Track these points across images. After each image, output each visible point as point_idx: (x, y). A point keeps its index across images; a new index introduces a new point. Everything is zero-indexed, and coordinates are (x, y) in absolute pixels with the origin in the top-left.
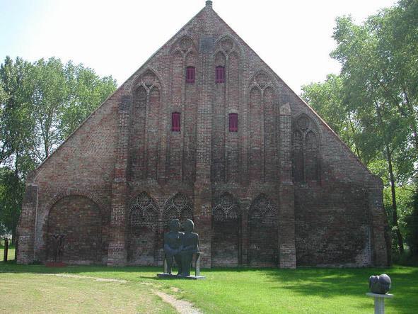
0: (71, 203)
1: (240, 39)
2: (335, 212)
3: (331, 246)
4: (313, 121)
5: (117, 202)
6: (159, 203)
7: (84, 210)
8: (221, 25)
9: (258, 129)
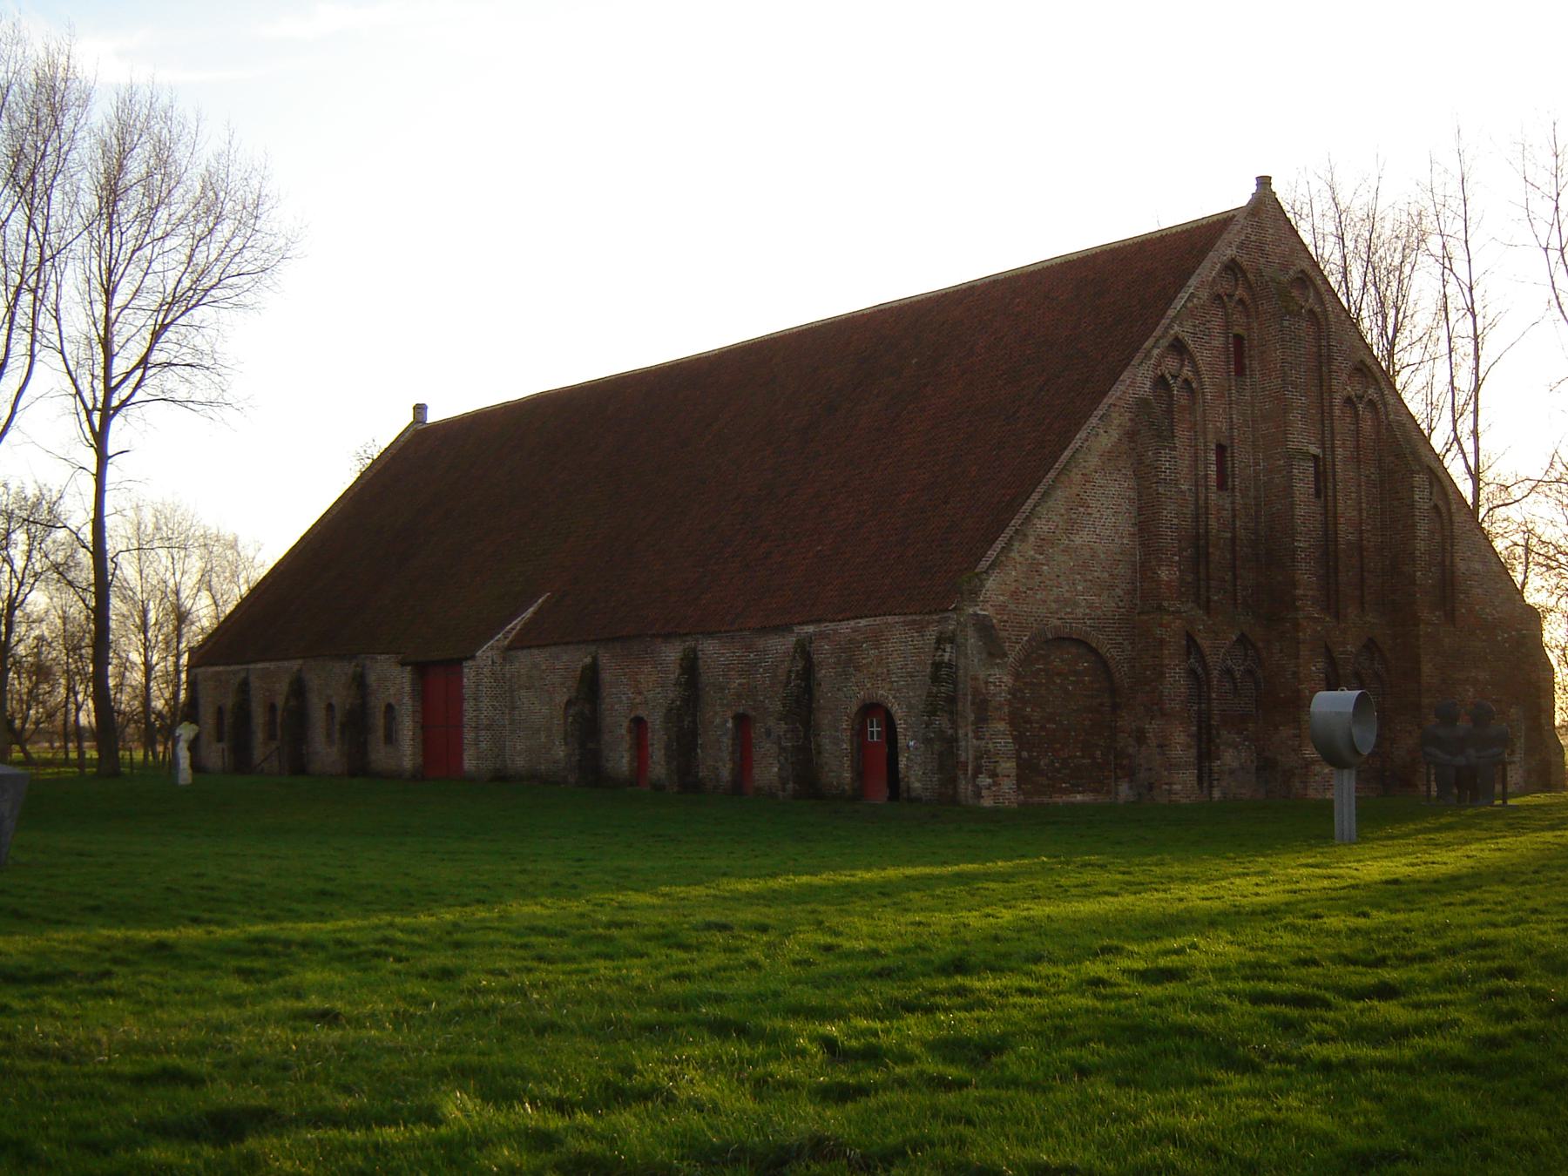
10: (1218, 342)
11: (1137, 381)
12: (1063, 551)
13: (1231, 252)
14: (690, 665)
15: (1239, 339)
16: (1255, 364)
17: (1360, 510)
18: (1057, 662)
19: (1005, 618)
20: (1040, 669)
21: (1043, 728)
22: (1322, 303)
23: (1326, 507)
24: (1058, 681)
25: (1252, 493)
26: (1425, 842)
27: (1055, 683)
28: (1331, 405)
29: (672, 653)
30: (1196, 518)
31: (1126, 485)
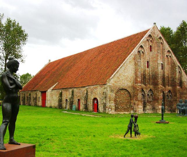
6: (146, 92)
10: (148, 46)
11: (135, 51)
13: (150, 33)
14: (73, 92)
15: (151, 46)
16: (153, 50)
21: (120, 102)
25: (152, 68)
29: (71, 90)
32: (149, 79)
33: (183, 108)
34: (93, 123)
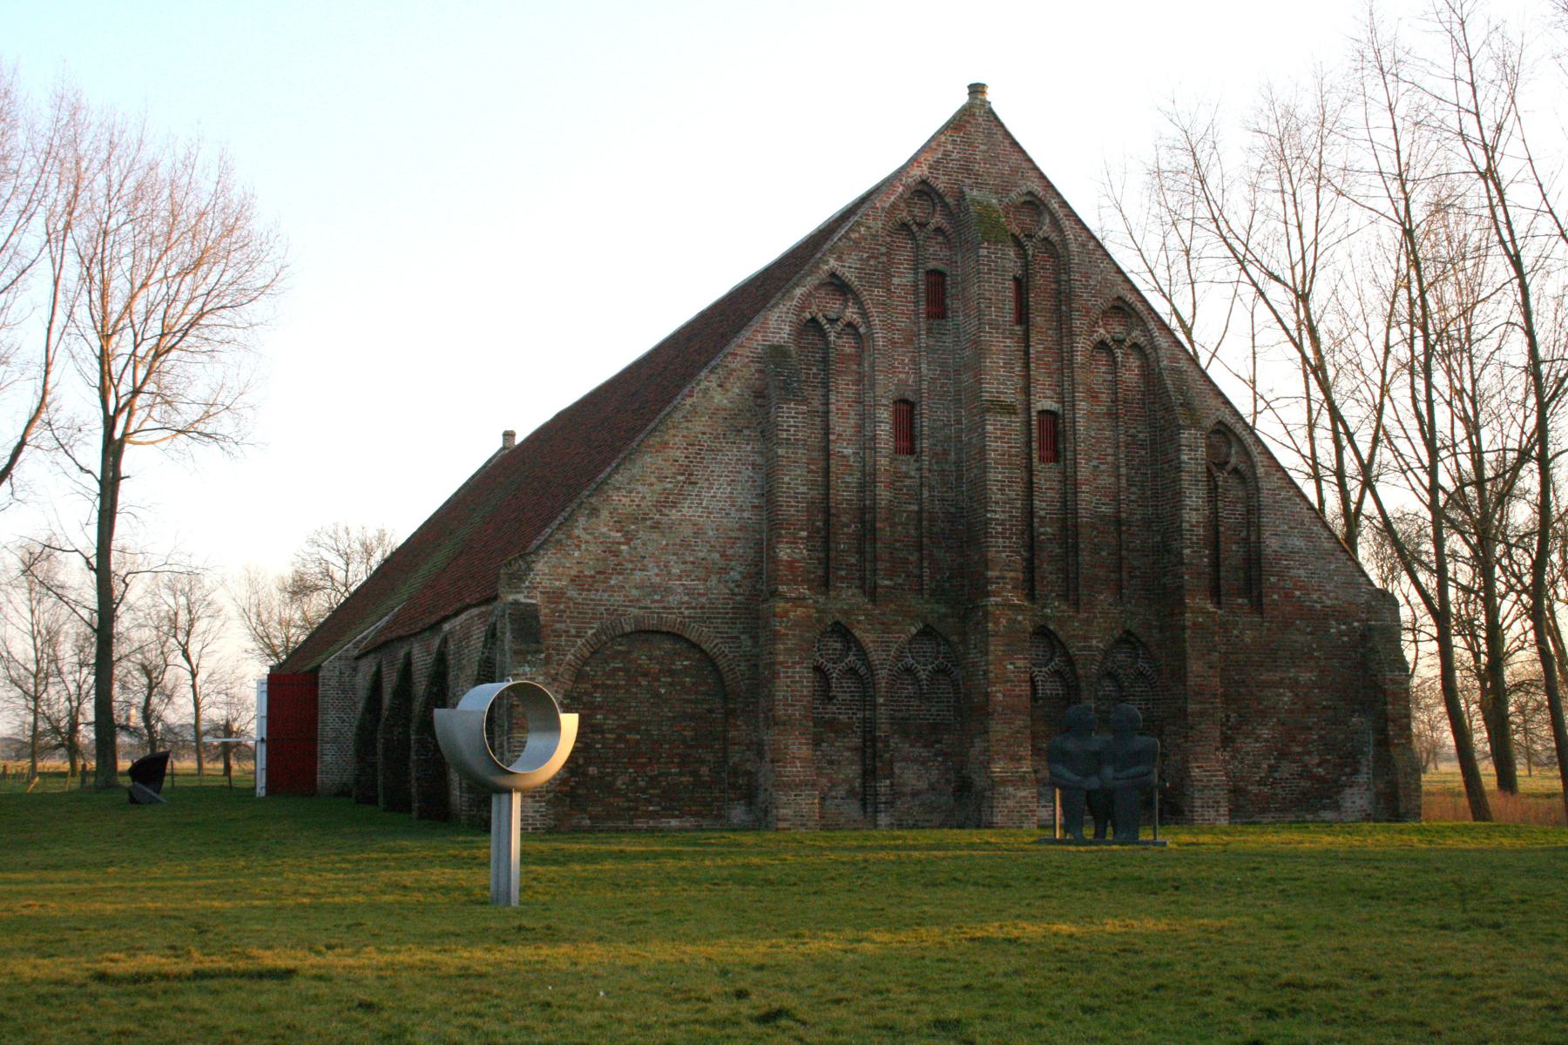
0: (635, 655)
1: (1064, 204)
2: (1296, 682)
3: (1287, 769)
4: (1240, 440)
5: (789, 651)
6: (876, 657)
7: (671, 673)
8: (1016, 156)
9: (1110, 459)
12: (652, 527)
16: (957, 304)
17: (1118, 477)
18: (643, 660)
19: (562, 607)
20: (620, 669)
21: (620, 738)
22: (1060, 229)
23: (1064, 473)
24: (644, 683)
25: (952, 457)
26: (1263, 866)
27: (639, 685)
28: (1072, 351)
30: (862, 487)
31: (749, 448)
32: (920, 547)
33: (1093, 783)
34: (1443, 927)
